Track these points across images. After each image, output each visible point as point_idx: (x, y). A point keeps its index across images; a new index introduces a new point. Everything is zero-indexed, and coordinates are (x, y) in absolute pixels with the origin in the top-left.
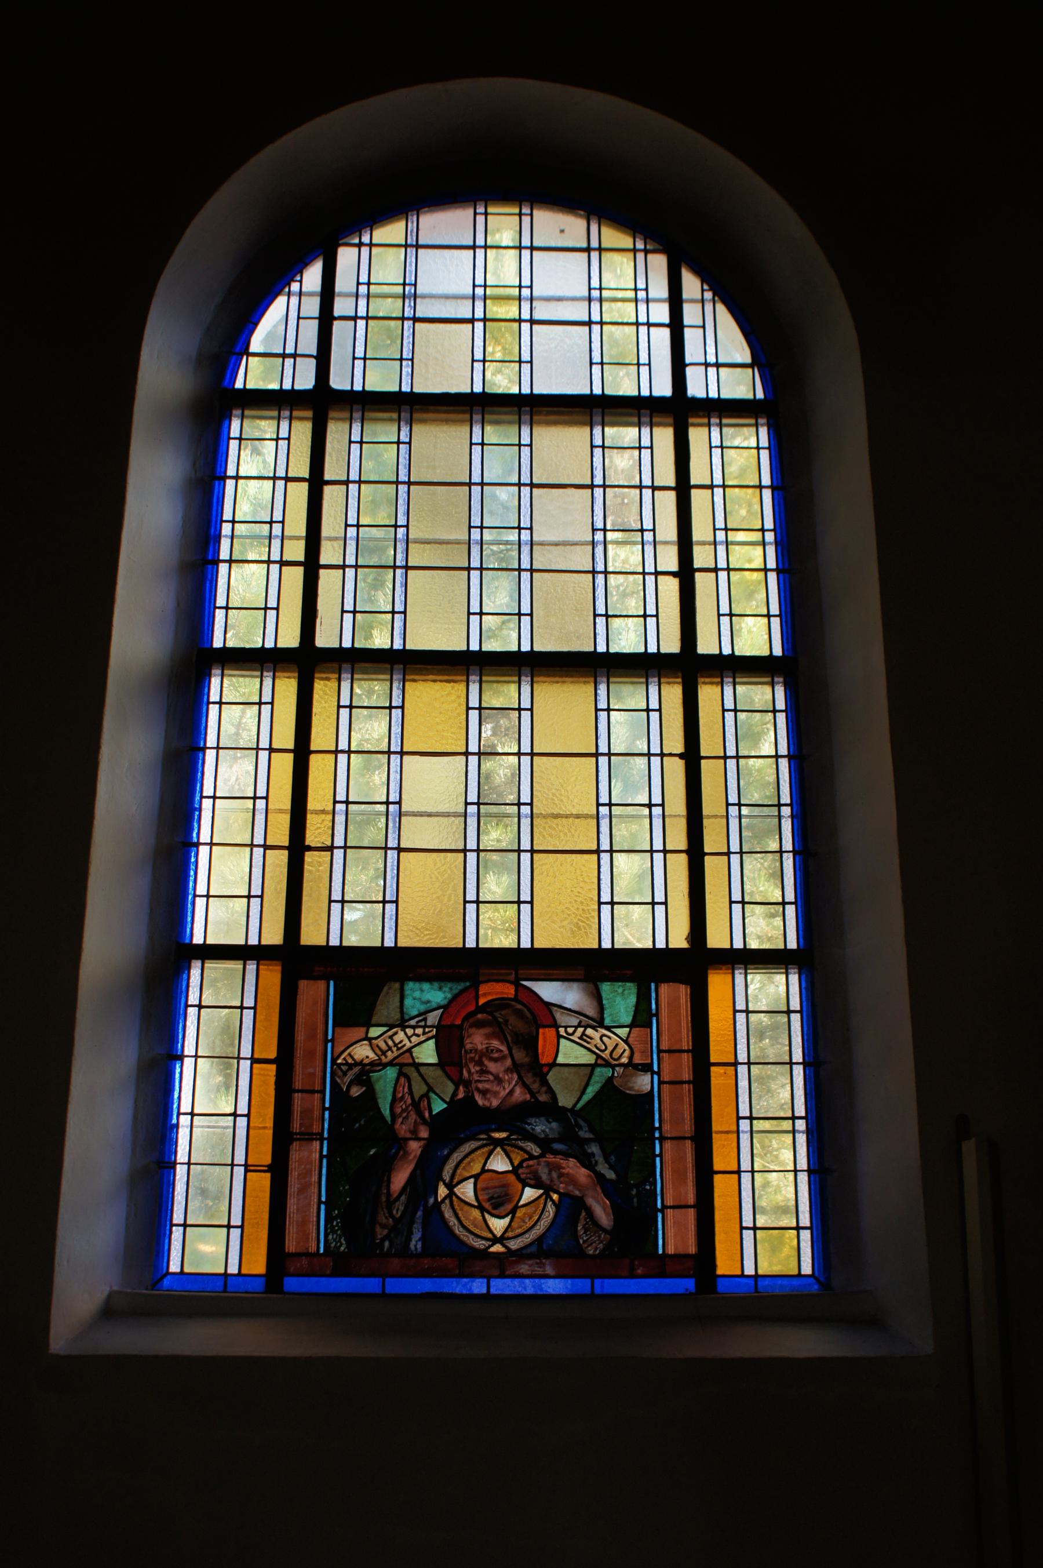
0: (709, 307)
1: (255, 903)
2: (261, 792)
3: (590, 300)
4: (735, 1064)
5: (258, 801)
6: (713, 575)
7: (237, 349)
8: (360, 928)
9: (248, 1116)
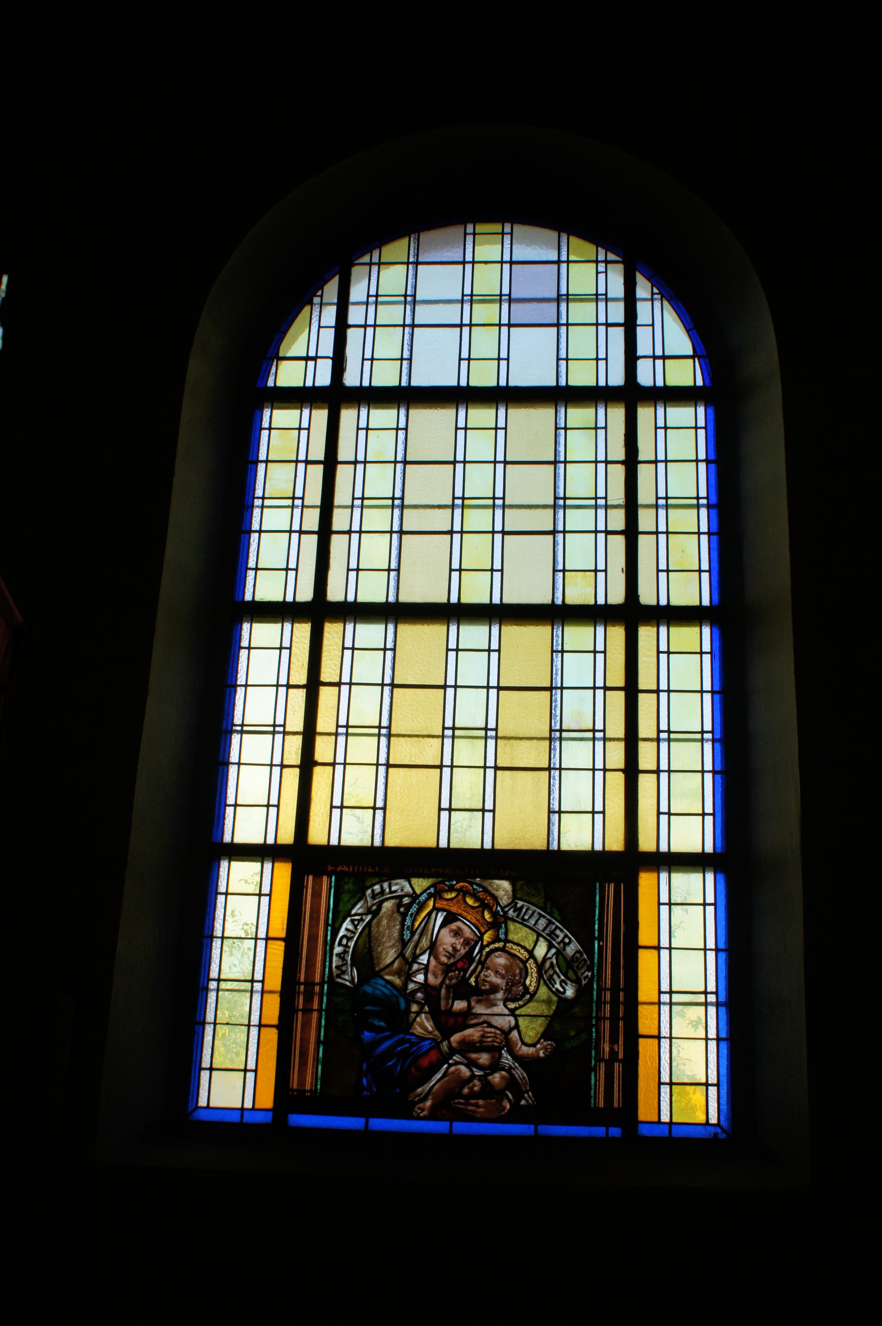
0: (657, 304)
3: (551, 739)
6: (653, 466)
7: (269, 355)
8: (356, 832)
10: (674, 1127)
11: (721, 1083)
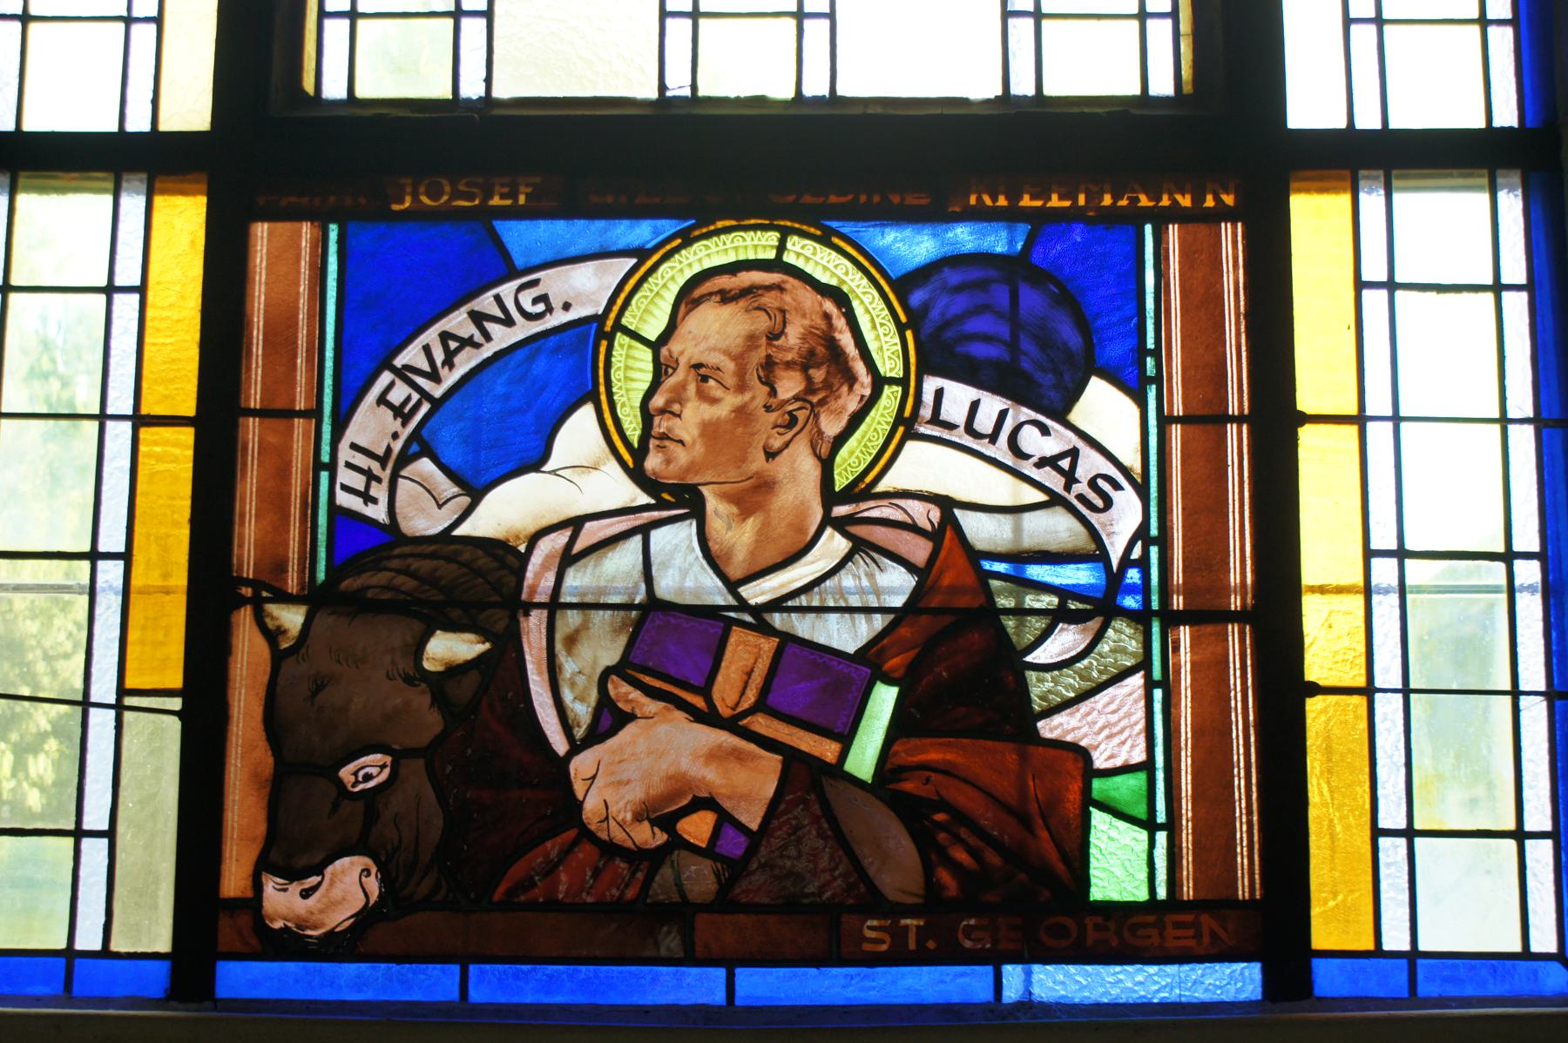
1: (126, 305)
2: (128, 274)
5: (102, 565)
9: (127, 556)
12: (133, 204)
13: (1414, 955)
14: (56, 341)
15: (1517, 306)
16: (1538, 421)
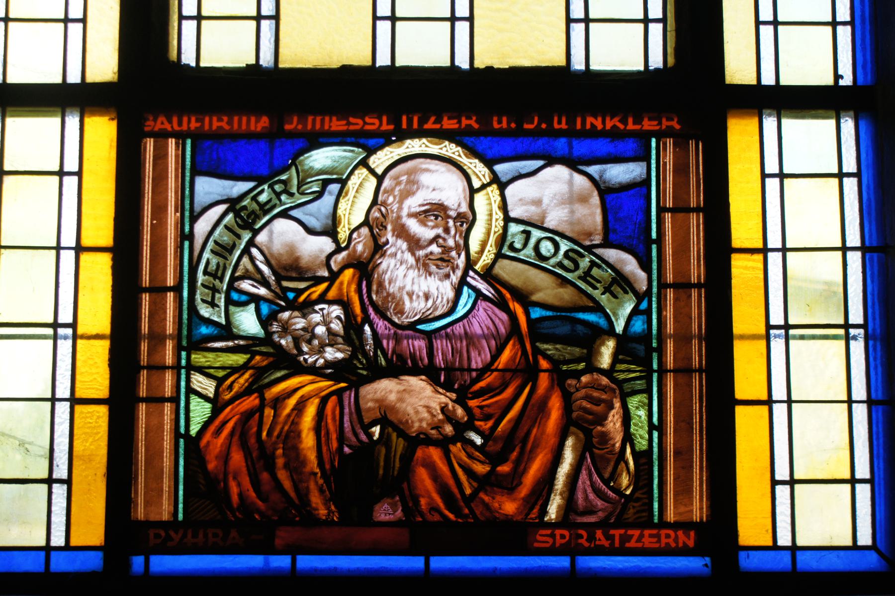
2: (66, 316)
4: (769, 402)
10: (799, 554)
11: (876, 479)
12: (73, 121)
13: (794, 549)
14: (32, 209)
15: (864, 492)
16: (870, 402)
